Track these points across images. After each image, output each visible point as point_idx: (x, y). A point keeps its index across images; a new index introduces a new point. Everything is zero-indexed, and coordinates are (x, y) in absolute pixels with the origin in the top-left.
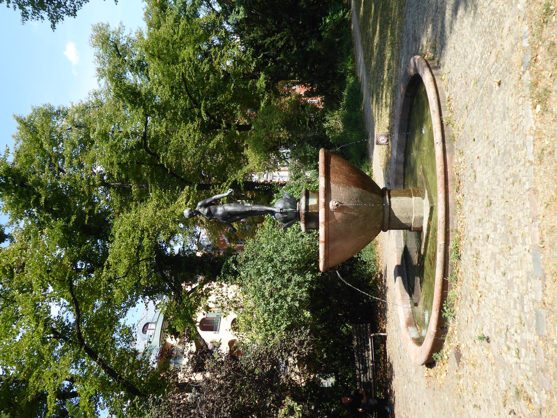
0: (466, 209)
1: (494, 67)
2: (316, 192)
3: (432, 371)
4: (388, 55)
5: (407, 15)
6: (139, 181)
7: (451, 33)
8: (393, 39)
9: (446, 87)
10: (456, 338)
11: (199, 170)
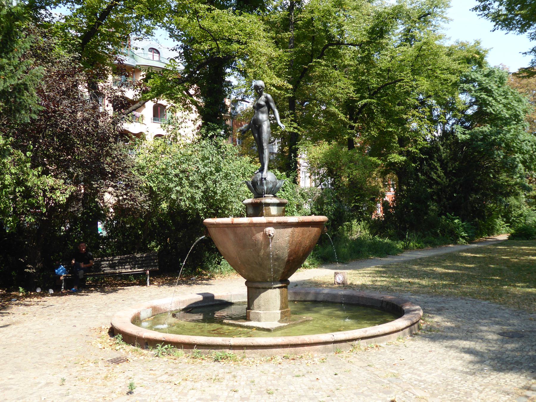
0: (266, 366)
1: (411, 395)
2: (284, 213)
3: (105, 333)
4: (424, 282)
5: (464, 301)
6: (297, 40)
7: (446, 347)
8: (440, 287)
9: (391, 344)
10: (136, 358)
11: (310, 100)
